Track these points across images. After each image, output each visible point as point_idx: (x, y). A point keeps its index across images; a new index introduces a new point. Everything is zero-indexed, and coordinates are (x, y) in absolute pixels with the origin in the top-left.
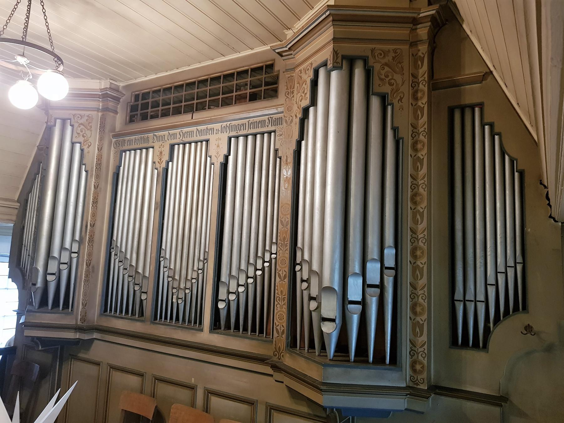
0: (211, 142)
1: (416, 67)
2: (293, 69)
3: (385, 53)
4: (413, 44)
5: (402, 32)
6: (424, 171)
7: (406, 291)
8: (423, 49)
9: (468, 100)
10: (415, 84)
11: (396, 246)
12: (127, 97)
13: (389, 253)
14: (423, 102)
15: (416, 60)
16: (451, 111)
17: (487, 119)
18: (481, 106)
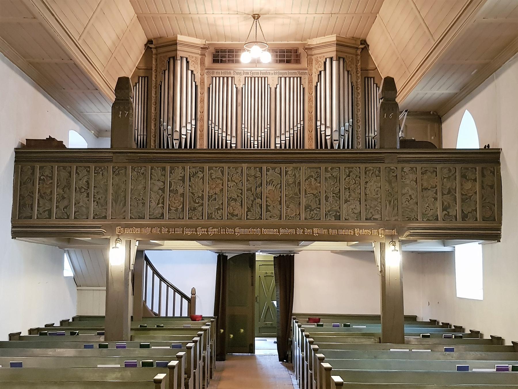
0: (302, 78)
1: (357, 63)
2: (312, 55)
3: (349, 57)
4: (357, 55)
5: (352, 51)
6: (360, 97)
7: (355, 133)
8: (359, 57)
9: (370, 76)
10: (357, 69)
11: (352, 119)
12: (212, 50)
13: (351, 120)
14: (359, 75)
15: (357, 61)
16: (365, 78)
17: (376, 82)
18: (374, 78)
